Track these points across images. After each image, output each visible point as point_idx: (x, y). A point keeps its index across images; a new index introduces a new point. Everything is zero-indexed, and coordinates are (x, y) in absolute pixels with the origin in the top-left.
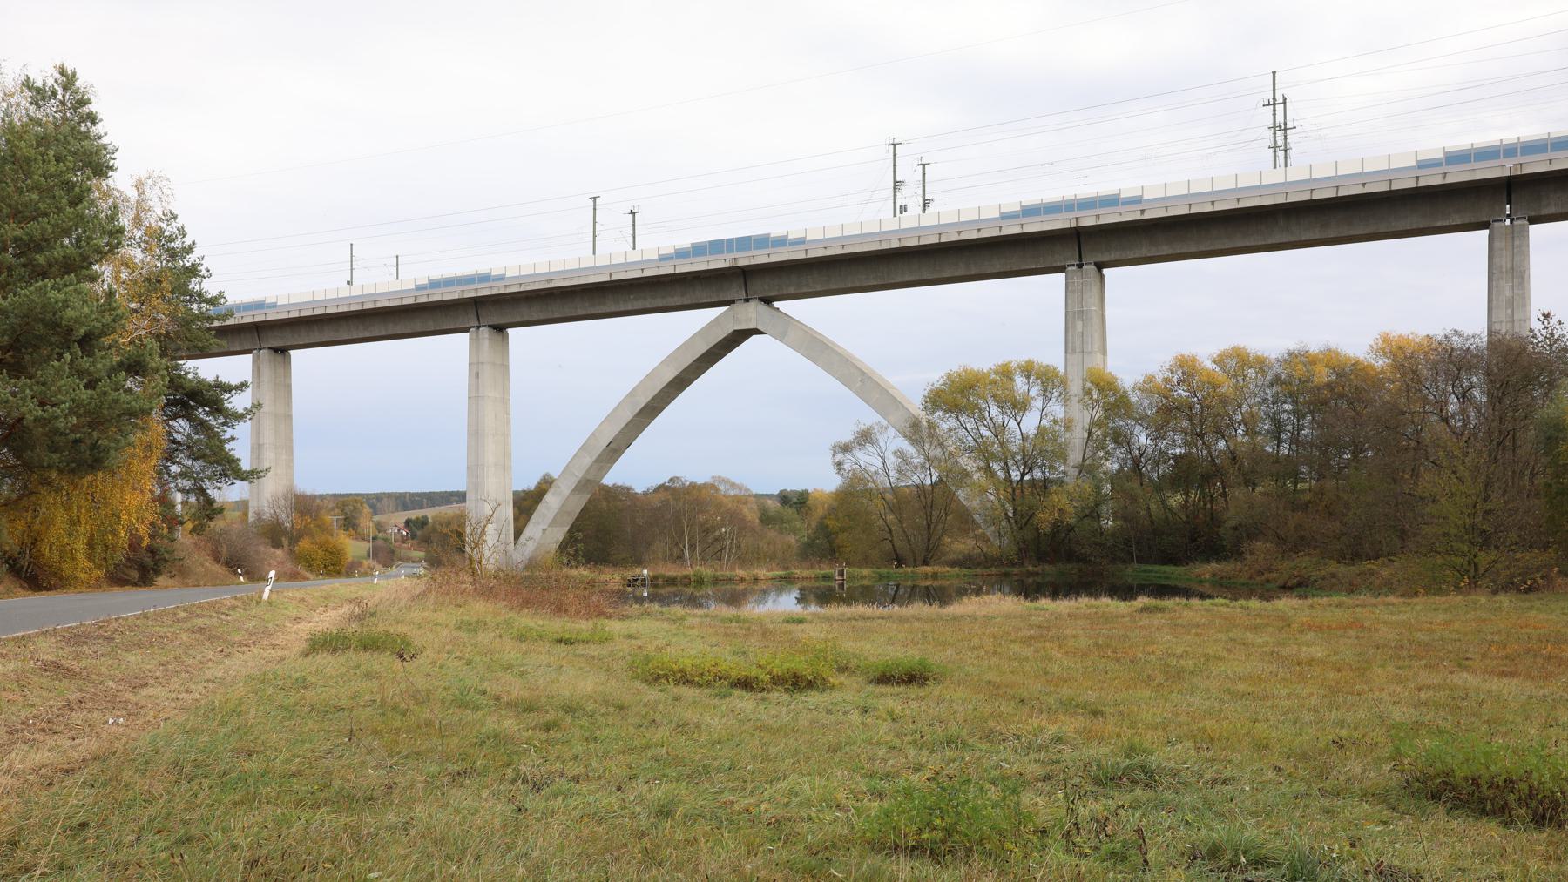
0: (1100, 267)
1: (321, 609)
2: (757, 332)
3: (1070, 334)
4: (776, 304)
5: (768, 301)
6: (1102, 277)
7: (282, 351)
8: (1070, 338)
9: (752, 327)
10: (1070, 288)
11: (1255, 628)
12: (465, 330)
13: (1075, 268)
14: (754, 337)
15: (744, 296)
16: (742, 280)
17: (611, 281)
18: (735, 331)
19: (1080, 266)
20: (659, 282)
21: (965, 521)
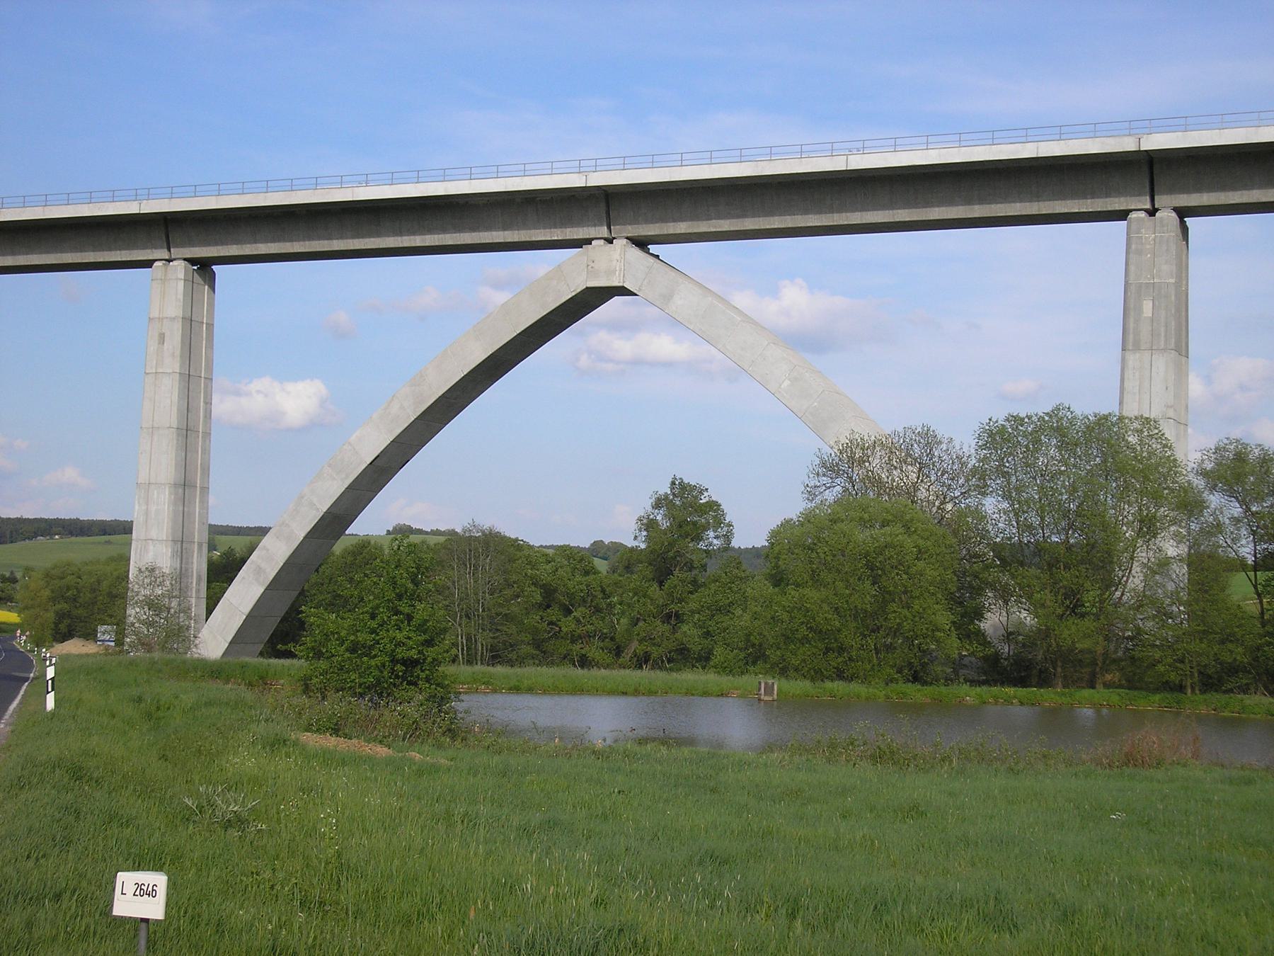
0: (1183, 213)
1: (114, 664)
2: (622, 291)
3: (1131, 321)
4: (653, 248)
5: (641, 244)
6: (1185, 230)
7: (204, 267)
8: (1131, 325)
9: (616, 284)
10: (1133, 246)
11: (722, 694)
12: (1122, 215)
13: (1143, 214)
14: (617, 300)
15: (1148, 206)
16: (603, 206)
17: (847, 170)
18: (587, 288)
19: (1152, 212)
20: (534, 199)
21: (334, 555)
